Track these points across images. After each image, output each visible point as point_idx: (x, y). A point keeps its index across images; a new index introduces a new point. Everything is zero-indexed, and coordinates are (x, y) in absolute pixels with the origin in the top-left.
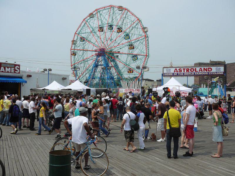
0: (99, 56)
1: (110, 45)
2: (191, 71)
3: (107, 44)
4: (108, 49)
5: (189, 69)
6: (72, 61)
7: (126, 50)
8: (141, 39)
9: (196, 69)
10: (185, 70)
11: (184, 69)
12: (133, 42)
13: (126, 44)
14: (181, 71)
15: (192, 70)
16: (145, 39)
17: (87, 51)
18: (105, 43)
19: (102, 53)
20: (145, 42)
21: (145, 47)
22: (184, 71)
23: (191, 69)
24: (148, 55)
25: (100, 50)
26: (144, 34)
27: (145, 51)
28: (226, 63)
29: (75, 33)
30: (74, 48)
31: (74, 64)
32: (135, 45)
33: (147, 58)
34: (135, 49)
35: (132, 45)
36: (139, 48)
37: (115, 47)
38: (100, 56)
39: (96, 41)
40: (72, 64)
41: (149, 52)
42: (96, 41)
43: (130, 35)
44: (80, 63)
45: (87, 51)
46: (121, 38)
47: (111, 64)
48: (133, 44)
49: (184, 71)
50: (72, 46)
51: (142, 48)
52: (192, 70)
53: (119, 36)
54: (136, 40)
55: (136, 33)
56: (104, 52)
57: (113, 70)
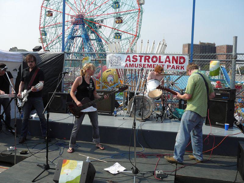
0: (76, 25)
1: (92, 11)
2: (152, 60)
3: (88, 10)
4: (87, 16)
5: (149, 57)
6: (41, 23)
7: (110, 22)
8: (132, 11)
9: (160, 57)
10: (143, 58)
11: (141, 57)
12: (122, 13)
13: (112, 15)
14: (133, 57)
15: (155, 59)
16: (138, 13)
17: (106, 26)
18: (86, 7)
19: (80, 20)
20: (137, 17)
21: (135, 24)
22: (141, 61)
23: (153, 57)
24: (138, 35)
25: (79, 15)
26: (137, 6)
27: (135, 30)
28: (216, 46)
29: (42, 7)
30: (47, 6)
31: (44, 27)
32: (125, 18)
33: (136, 39)
34: (123, 24)
35: (119, 18)
36: (129, 23)
37: (97, 16)
38: (78, 24)
39: (75, 3)
40: (41, 27)
41: (140, 31)
42: (75, 3)
43: (120, 4)
44: (51, 27)
45: (106, 26)
46: (107, 5)
47: (92, 36)
48: (122, 16)
49: (141, 61)
50: (44, 2)
51: (132, 24)
52: (155, 59)
53: (105, 3)
54: (127, 13)
55: (128, 3)
56: (83, 19)
57: (95, 44)
